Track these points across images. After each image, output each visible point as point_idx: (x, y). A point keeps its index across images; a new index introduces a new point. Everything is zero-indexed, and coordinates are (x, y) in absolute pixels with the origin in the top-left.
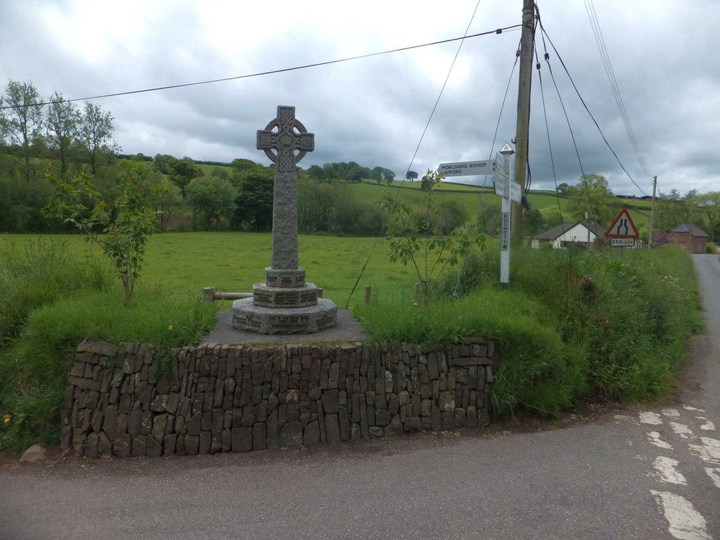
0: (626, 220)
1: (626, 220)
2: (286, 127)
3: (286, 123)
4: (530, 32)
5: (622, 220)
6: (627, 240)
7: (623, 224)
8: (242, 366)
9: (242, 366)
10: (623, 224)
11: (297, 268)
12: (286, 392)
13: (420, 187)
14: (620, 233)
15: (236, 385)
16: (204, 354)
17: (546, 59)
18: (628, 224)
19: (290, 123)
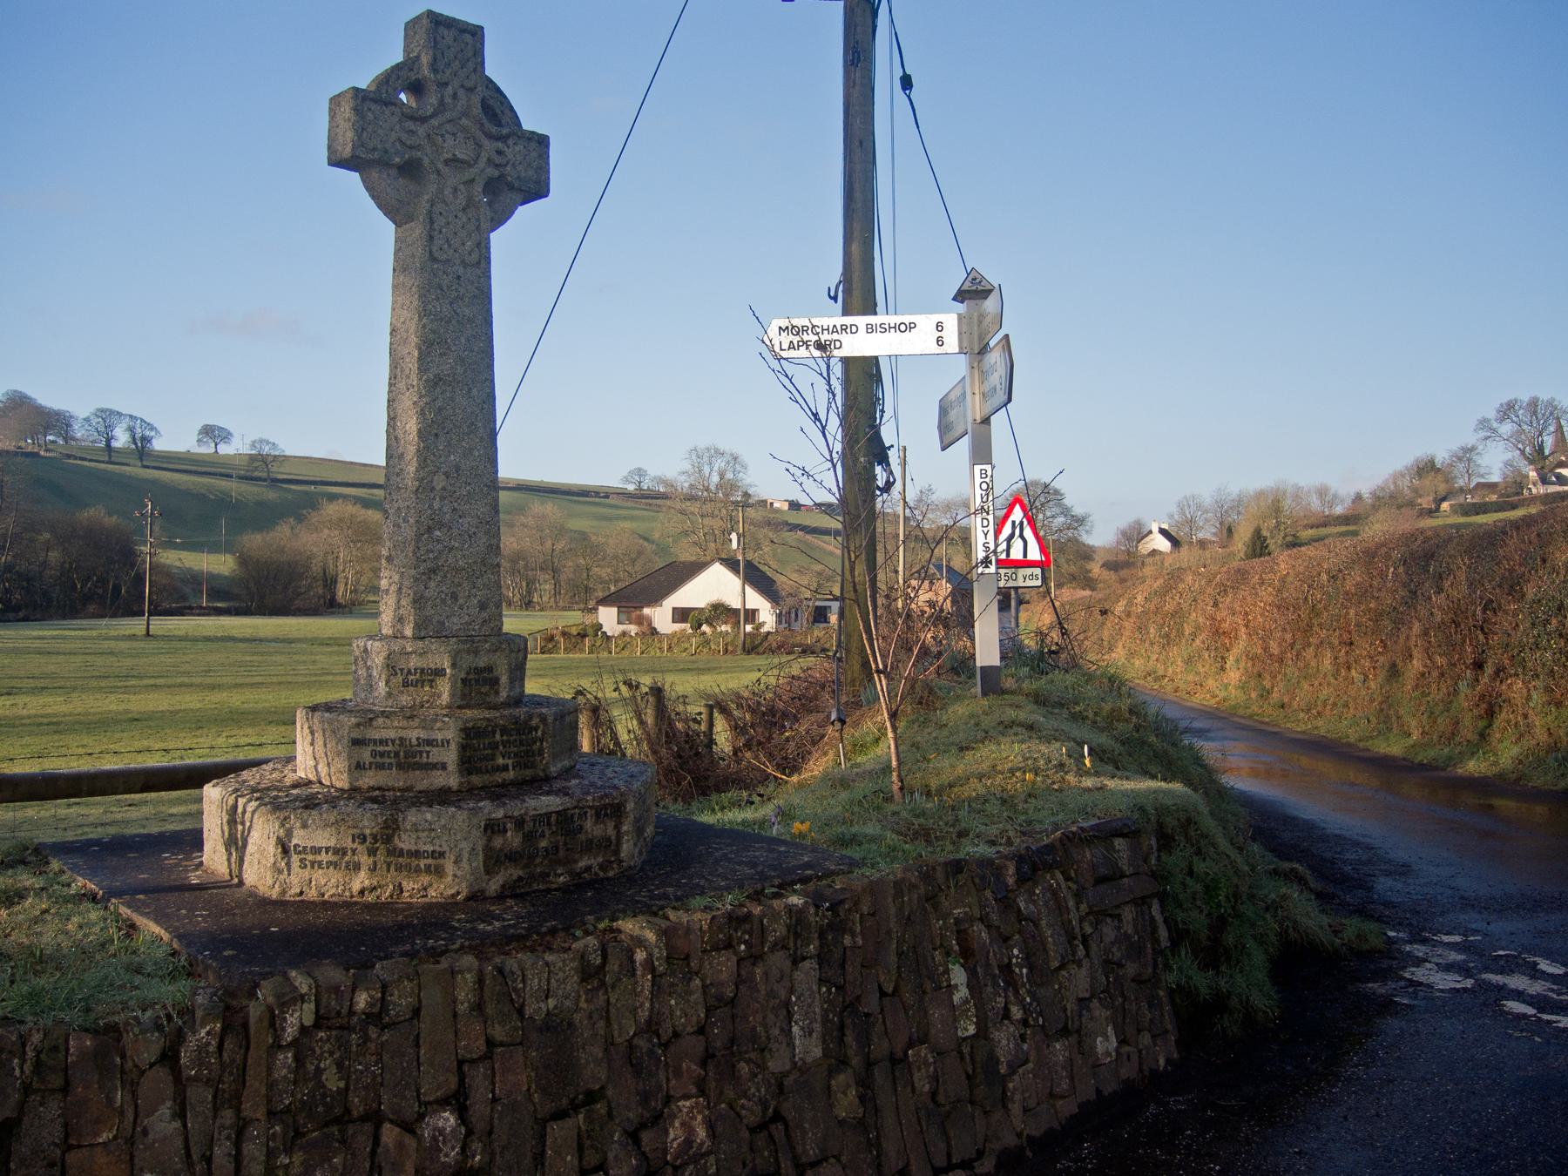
0: (1021, 523)
1: (1021, 523)
2: (455, 96)
3: (456, 83)
4: (868, 13)
5: (1014, 522)
6: (1029, 571)
7: (1017, 532)
8: (490, 1043)
9: (490, 1043)
10: (1017, 532)
11: (1451, 505)
12: (657, 1120)
13: (957, 350)
14: (1030, 557)
15: (470, 1132)
16: (309, 1020)
17: (904, 89)
18: (1028, 533)
19: (469, 84)
